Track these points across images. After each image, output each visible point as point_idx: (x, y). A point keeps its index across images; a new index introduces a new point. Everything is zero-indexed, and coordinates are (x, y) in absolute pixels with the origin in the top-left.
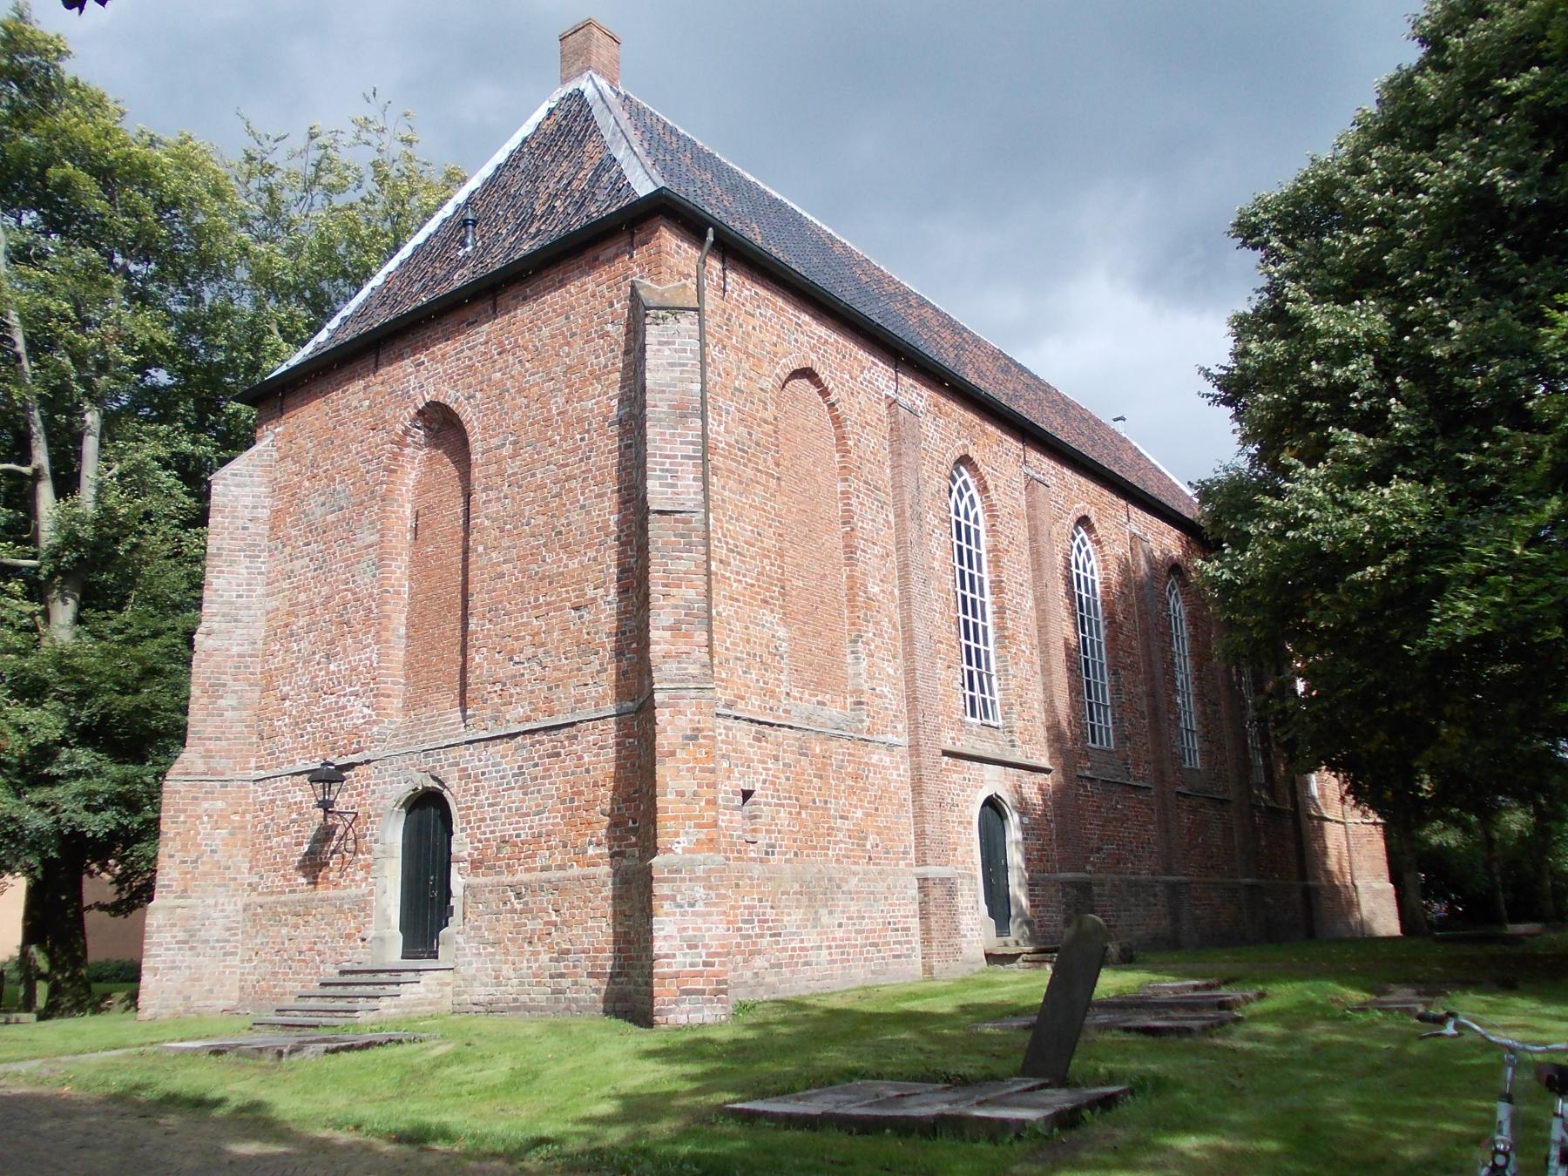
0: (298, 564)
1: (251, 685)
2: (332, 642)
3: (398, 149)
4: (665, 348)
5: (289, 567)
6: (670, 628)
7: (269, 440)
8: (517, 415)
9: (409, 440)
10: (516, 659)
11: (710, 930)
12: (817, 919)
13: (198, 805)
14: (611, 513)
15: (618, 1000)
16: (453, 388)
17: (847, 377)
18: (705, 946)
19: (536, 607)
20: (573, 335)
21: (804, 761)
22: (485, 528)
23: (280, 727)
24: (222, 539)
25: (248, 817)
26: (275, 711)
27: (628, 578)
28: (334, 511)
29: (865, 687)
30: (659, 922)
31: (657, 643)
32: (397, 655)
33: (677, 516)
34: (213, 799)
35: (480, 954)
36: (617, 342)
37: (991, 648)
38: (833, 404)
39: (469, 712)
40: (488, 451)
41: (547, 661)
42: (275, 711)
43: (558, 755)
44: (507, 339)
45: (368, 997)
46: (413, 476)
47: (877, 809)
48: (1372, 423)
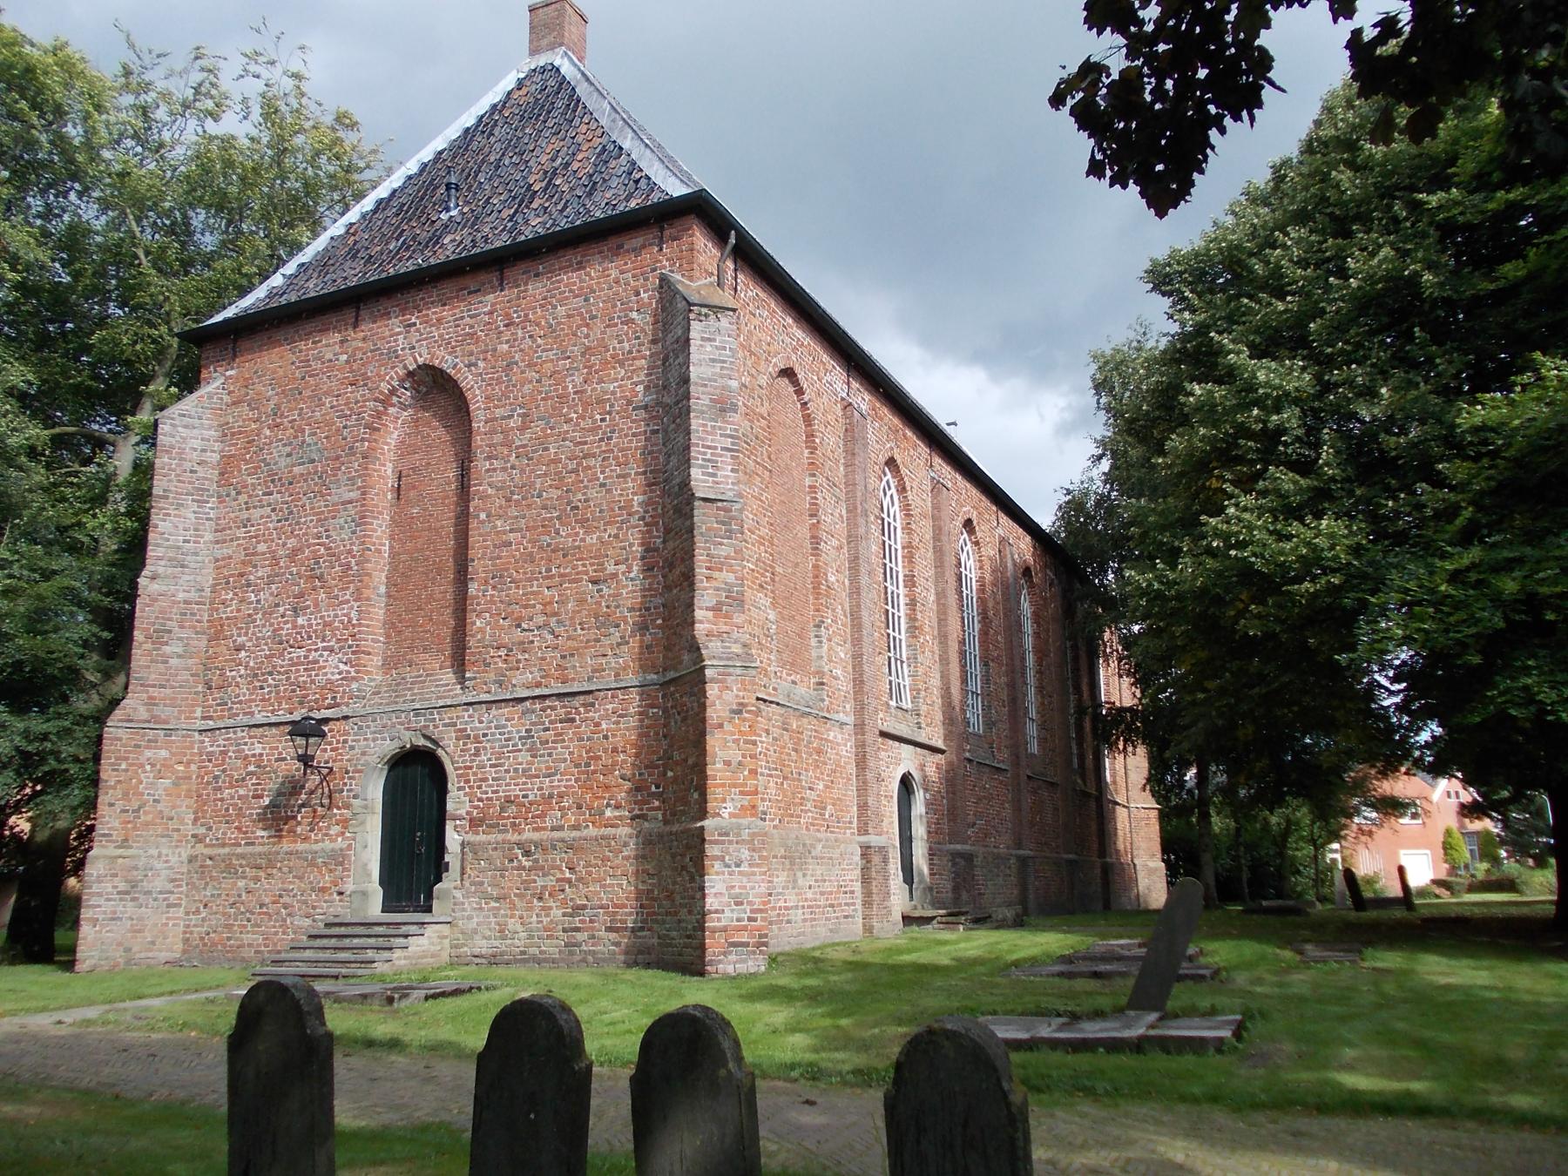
1: (197, 633)
2: (301, 595)
3: (288, 84)
5: (244, 514)
7: (216, 384)
8: (527, 388)
9: (395, 399)
10: (524, 626)
11: (753, 888)
12: (795, 881)
13: (141, 753)
14: (634, 494)
15: (640, 952)
16: (450, 354)
20: (593, 317)
21: (786, 735)
22: (489, 496)
23: (234, 678)
24: (170, 481)
25: (193, 767)
27: (653, 557)
28: (304, 463)
29: (826, 669)
30: (710, 881)
32: (377, 614)
33: (720, 504)
34: (156, 748)
35: (481, 908)
36: (643, 330)
37: (903, 637)
38: (806, 403)
39: (468, 675)
40: (492, 420)
41: (559, 630)
42: (226, 661)
43: (573, 720)
44: (515, 312)
45: (378, 949)
46: (395, 436)
48: (1304, 467)
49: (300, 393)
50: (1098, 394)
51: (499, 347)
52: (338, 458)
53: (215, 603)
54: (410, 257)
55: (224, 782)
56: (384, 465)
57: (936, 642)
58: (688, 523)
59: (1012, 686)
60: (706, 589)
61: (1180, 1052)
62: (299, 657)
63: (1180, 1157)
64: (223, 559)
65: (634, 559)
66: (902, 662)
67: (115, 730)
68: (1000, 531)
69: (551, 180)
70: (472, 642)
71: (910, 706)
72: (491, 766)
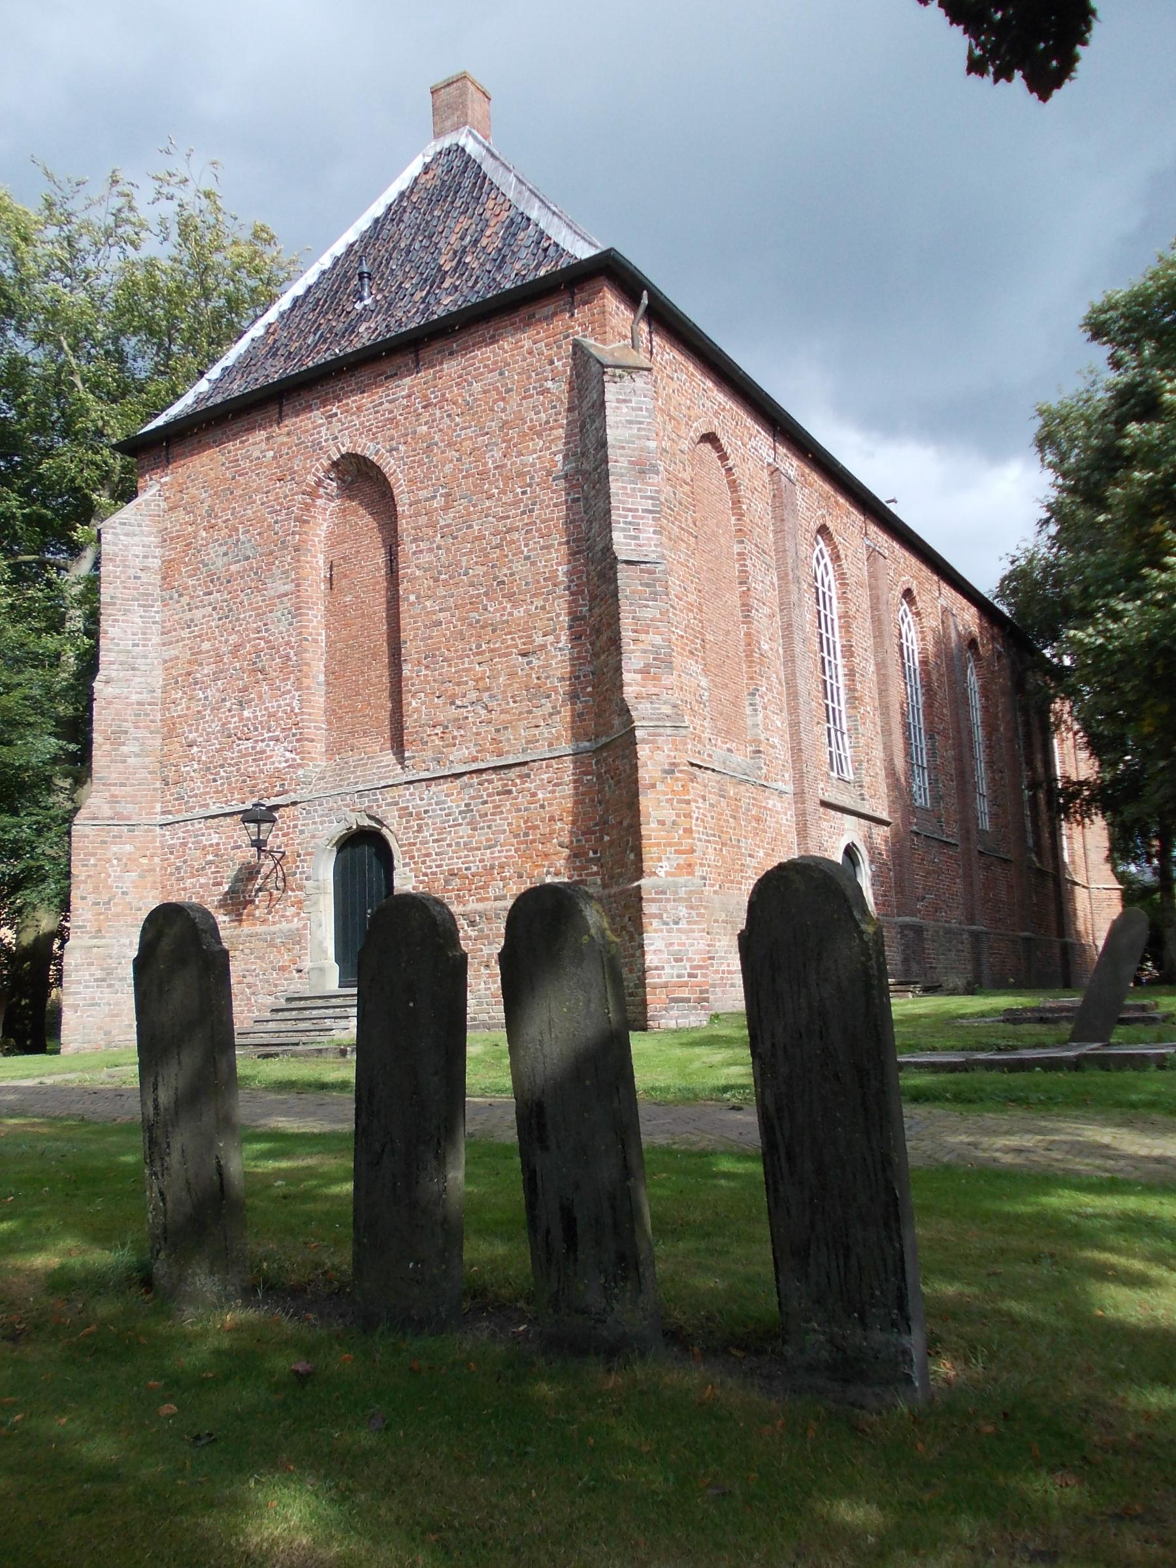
0: (198, 614)
2: (245, 689)
4: (623, 405)
6: (640, 672)
8: (448, 468)
9: (321, 491)
14: (559, 564)
16: (372, 440)
17: (739, 443)
18: (689, 960)
19: (478, 654)
20: (508, 391)
21: (723, 802)
23: (188, 773)
24: (116, 588)
25: (157, 860)
26: (180, 757)
27: (580, 626)
28: (239, 561)
29: (762, 738)
30: (650, 938)
31: (630, 685)
36: (559, 399)
37: (843, 707)
38: (731, 469)
39: (407, 754)
41: (492, 704)
42: (180, 757)
43: (509, 792)
44: (433, 392)
46: (324, 527)
47: (773, 850)
49: (232, 493)
50: (1041, 449)
51: (418, 429)
52: (271, 552)
53: (167, 703)
54: (328, 349)
55: (186, 872)
56: (315, 557)
57: (878, 713)
58: (612, 587)
59: (959, 759)
60: (633, 652)
61: (1120, 1068)
62: (247, 749)
63: (1106, 1140)
64: (171, 660)
65: (562, 629)
66: (843, 733)
67: (81, 827)
68: (942, 601)
69: (461, 258)
70: (408, 722)
71: (852, 777)
72: (434, 841)
